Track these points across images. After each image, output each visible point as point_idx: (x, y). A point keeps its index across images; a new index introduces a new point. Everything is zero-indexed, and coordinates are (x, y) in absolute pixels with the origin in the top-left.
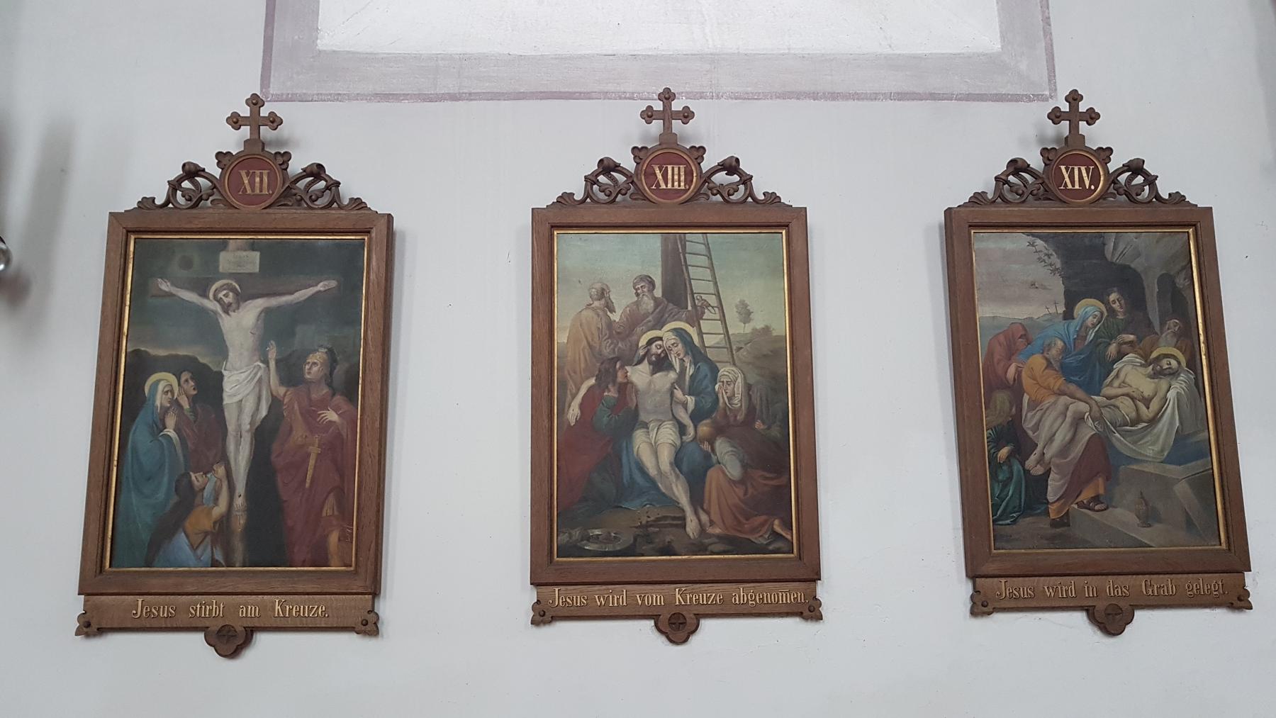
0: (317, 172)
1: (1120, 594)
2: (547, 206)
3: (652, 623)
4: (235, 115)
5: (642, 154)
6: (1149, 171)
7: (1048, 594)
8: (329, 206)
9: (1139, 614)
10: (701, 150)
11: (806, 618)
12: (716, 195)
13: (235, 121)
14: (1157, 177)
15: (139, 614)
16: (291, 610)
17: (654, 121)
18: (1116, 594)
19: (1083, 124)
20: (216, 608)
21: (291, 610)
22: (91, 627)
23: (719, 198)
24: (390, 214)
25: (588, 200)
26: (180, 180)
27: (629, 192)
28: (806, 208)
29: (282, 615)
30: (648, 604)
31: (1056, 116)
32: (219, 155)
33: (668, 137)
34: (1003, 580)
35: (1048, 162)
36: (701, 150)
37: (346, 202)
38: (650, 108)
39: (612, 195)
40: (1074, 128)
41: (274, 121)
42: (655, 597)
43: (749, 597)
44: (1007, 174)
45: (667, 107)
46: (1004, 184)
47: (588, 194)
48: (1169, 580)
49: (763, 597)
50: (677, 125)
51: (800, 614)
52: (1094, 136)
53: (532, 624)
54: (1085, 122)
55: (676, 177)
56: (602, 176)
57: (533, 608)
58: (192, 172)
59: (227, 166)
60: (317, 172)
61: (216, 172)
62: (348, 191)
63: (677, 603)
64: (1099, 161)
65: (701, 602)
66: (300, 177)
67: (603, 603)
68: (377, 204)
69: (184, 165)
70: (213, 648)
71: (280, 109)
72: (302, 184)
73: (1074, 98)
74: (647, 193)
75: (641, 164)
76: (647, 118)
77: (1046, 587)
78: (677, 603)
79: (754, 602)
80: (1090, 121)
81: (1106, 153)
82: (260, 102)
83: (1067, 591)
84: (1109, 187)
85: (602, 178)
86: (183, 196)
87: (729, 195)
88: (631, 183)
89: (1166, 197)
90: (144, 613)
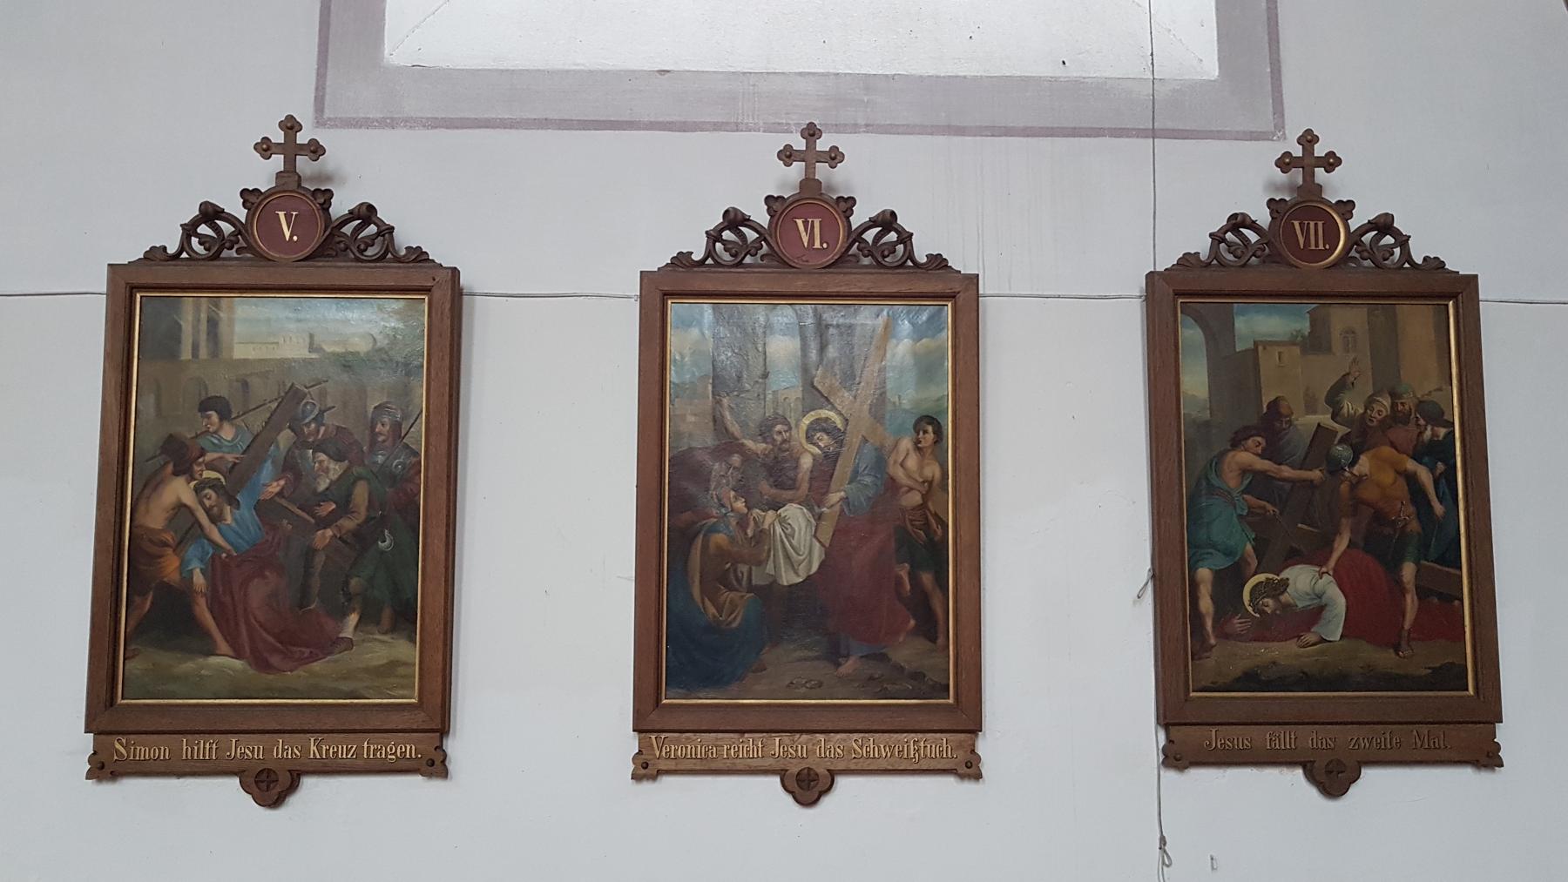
0: (366, 213)
2: (659, 269)
3: (236, 781)
4: (266, 139)
8: (382, 258)
9: (842, 782)
11: (962, 777)
13: (787, 155)
14: (1410, 237)
15: (233, 754)
16: (676, 750)
17: (794, 163)
18: (1320, 746)
19: (1320, 172)
20: (187, 749)
21: (676, 750)
22: (645, 770)
24: (455, 268)
26: (195, 223)
27: (761, 252)
29: (318, 757)
30: (154, 756)
32: (244, 192)
36: (850, 203)
37: (403, 252)
38: (788, 147)
39: (217, 246)
40: (1309, 175)
41: (315, 150)
42: (689, 747)
43: (388, 750)
44: (1224, 230)
45: (811, 144)
47: (710, 252)
48: (945, 740)
49: (738, 751)
50: (303, 164)
53: (632, 778)
57: (90, 761)
58: (210, 213)
59: (779, 213)
60: (366, 213)
61: (241, 214)
62: (405, 238)
67: (1367, 745)
68: (440, 254)
69: (726, 213)
70: (250, 796)
71: (843, 142)
72: (348, 229)
73: (1308, 139)
78: (312, 757)
79: (394, 757)
80: (1328, 168)
81: (1347, 208)
82: (817, 132)
84: (1351, 249)
85: (727, 235)
86: (200, 243)
89: (1419, 261)
90: (781, 754)
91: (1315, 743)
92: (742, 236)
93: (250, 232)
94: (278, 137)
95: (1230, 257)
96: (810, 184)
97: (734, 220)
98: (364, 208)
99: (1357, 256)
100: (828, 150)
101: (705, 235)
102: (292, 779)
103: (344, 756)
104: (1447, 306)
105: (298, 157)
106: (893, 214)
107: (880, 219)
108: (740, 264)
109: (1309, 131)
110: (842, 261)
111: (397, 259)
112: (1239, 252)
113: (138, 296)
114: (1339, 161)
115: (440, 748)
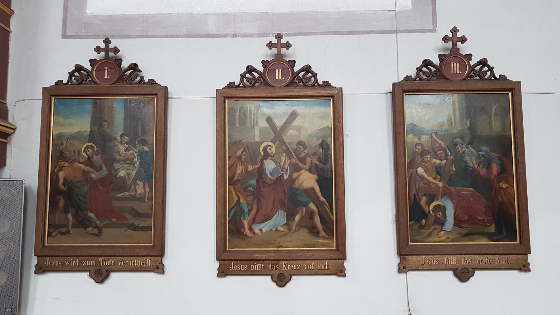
1: (467, 263)
2: (222, 88)
5: (266, 64)
6: (490, 65)
7: (66, 264)
10: (470, 55)
12: (300, 83)
14: (494, 67)
18: (466, 263)
20: (139, 262)
23: (478, 78)
25: (418, 79)
28: (342, 88)
31: (270, 45)
33: (279, 57)
34: (424, 256)
35: (441, 61)
38: (270, 42)
40: (454, 44)
44: (422, 67)
46: (420, 71)
47: (241, 81)
50: (283, 50)
51: (520, 270)
52: (464, 49)
54: (460, 42)
55: (455, 68)
56: (248, 74)
63: (284, 269)
64: (466, 60)
65: (294, 269)
66: (298, 73)
67: (68, 264)
70: (93, 279)
71: (291, 40)
73: (455, 30)
74: (270, 82)
75: (266, 68)
76: (270, 47)
77: (66, 262)
83: (75, 263)
85: (248, 75)
87: (306, 82)
88: (261, 77)
89: (498, 77)
91: (464, 262)
92: (253, 76)
93: (265, 76)
94: (459, 35)
95: (425, 77)
96: (279, 57)
97: (250, 69)
98: (308, 66)
99: (474, 75)
100: (285, 43)
101: (240, 76)
102: (107, 273)
103: (296, 269)
104: (509, 93)
105: (110, 53)
106: (310, 67)
107: (305, 68)
108: (253, 86)
109: (455, 28)
110: (291, 84)
111: (319, 85)
112: (428, 75)
113: (227, 101)
114: (466, 40)
115: (161, 263)
